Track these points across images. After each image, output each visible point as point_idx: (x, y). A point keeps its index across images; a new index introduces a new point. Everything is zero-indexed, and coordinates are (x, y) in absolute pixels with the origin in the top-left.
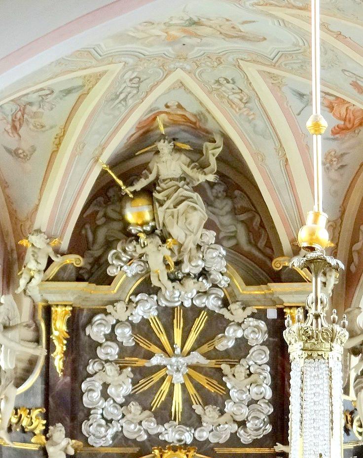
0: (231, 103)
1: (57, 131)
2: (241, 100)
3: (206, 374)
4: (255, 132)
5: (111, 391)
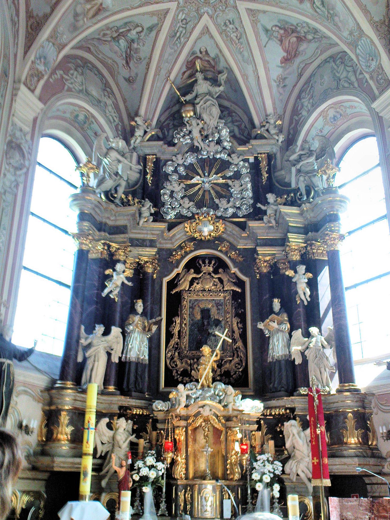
0: (231, 39)
1: (147, 60)
2: (237, 37)
3: (220, 186)
4: (243, 60)
5: (175, 195)
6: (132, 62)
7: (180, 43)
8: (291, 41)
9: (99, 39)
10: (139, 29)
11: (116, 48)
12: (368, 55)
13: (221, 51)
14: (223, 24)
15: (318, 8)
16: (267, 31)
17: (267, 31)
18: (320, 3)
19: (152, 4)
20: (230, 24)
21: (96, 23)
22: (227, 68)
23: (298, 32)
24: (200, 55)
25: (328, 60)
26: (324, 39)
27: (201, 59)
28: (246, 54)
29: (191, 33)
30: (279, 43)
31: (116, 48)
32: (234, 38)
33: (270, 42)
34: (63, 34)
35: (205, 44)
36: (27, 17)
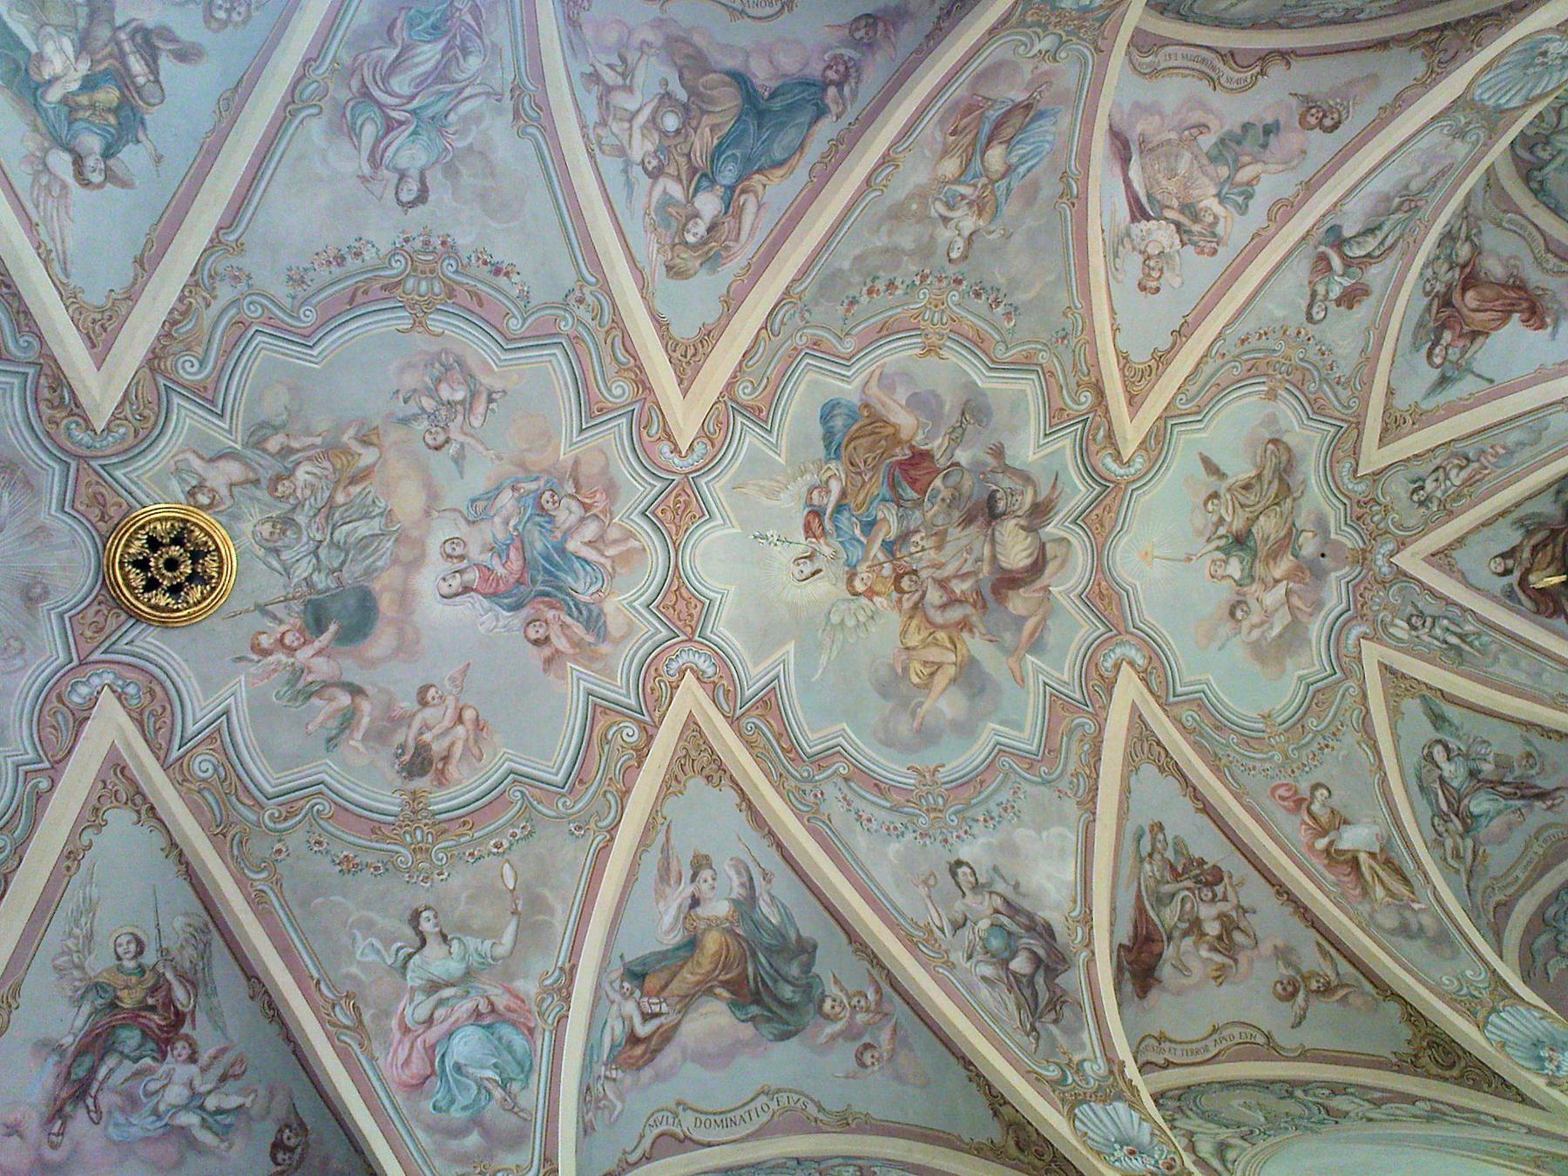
0: (1470, 482)
2: (1462, 468)
4: (1534, 443)
6: (1538, 782)
7: (1478, 635)
8: (1474, 304)
9: (1471, 873)
10: (1439, 753)
11: (1496, 825)
12: (1531, 71)
13: (1503, 514)
14: (1423, 510)
15: (1382, 243)
16: (1443, 381)
17: (1443, 381)
18: (1370, 239)
19: (1368, 712)
20: (1422, 488)
21: (1426, 875)
22: (1558, 492)
23: (1449, 287)
24: (1517, 574)
25: (1535, 186)
26: (1470, 210)
27: (1528, 571)
28: (1513, 438)
29: (1449, 602)
30: (1481, 339)
31: (1496, 825)
32: (1464, 474)
33: (1476, 367)
34: (1461, 978)
35: (1480, 560)
36: (1416, 1074)
